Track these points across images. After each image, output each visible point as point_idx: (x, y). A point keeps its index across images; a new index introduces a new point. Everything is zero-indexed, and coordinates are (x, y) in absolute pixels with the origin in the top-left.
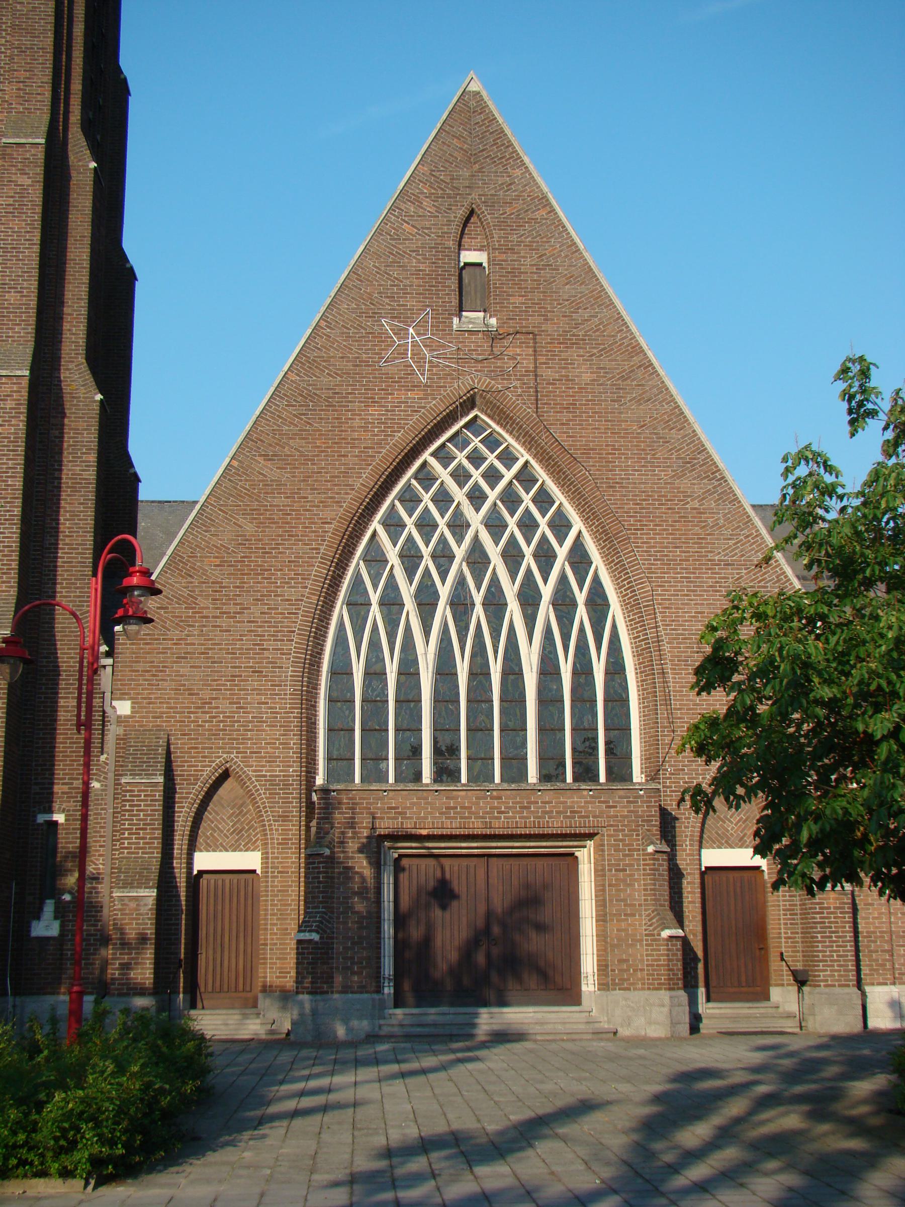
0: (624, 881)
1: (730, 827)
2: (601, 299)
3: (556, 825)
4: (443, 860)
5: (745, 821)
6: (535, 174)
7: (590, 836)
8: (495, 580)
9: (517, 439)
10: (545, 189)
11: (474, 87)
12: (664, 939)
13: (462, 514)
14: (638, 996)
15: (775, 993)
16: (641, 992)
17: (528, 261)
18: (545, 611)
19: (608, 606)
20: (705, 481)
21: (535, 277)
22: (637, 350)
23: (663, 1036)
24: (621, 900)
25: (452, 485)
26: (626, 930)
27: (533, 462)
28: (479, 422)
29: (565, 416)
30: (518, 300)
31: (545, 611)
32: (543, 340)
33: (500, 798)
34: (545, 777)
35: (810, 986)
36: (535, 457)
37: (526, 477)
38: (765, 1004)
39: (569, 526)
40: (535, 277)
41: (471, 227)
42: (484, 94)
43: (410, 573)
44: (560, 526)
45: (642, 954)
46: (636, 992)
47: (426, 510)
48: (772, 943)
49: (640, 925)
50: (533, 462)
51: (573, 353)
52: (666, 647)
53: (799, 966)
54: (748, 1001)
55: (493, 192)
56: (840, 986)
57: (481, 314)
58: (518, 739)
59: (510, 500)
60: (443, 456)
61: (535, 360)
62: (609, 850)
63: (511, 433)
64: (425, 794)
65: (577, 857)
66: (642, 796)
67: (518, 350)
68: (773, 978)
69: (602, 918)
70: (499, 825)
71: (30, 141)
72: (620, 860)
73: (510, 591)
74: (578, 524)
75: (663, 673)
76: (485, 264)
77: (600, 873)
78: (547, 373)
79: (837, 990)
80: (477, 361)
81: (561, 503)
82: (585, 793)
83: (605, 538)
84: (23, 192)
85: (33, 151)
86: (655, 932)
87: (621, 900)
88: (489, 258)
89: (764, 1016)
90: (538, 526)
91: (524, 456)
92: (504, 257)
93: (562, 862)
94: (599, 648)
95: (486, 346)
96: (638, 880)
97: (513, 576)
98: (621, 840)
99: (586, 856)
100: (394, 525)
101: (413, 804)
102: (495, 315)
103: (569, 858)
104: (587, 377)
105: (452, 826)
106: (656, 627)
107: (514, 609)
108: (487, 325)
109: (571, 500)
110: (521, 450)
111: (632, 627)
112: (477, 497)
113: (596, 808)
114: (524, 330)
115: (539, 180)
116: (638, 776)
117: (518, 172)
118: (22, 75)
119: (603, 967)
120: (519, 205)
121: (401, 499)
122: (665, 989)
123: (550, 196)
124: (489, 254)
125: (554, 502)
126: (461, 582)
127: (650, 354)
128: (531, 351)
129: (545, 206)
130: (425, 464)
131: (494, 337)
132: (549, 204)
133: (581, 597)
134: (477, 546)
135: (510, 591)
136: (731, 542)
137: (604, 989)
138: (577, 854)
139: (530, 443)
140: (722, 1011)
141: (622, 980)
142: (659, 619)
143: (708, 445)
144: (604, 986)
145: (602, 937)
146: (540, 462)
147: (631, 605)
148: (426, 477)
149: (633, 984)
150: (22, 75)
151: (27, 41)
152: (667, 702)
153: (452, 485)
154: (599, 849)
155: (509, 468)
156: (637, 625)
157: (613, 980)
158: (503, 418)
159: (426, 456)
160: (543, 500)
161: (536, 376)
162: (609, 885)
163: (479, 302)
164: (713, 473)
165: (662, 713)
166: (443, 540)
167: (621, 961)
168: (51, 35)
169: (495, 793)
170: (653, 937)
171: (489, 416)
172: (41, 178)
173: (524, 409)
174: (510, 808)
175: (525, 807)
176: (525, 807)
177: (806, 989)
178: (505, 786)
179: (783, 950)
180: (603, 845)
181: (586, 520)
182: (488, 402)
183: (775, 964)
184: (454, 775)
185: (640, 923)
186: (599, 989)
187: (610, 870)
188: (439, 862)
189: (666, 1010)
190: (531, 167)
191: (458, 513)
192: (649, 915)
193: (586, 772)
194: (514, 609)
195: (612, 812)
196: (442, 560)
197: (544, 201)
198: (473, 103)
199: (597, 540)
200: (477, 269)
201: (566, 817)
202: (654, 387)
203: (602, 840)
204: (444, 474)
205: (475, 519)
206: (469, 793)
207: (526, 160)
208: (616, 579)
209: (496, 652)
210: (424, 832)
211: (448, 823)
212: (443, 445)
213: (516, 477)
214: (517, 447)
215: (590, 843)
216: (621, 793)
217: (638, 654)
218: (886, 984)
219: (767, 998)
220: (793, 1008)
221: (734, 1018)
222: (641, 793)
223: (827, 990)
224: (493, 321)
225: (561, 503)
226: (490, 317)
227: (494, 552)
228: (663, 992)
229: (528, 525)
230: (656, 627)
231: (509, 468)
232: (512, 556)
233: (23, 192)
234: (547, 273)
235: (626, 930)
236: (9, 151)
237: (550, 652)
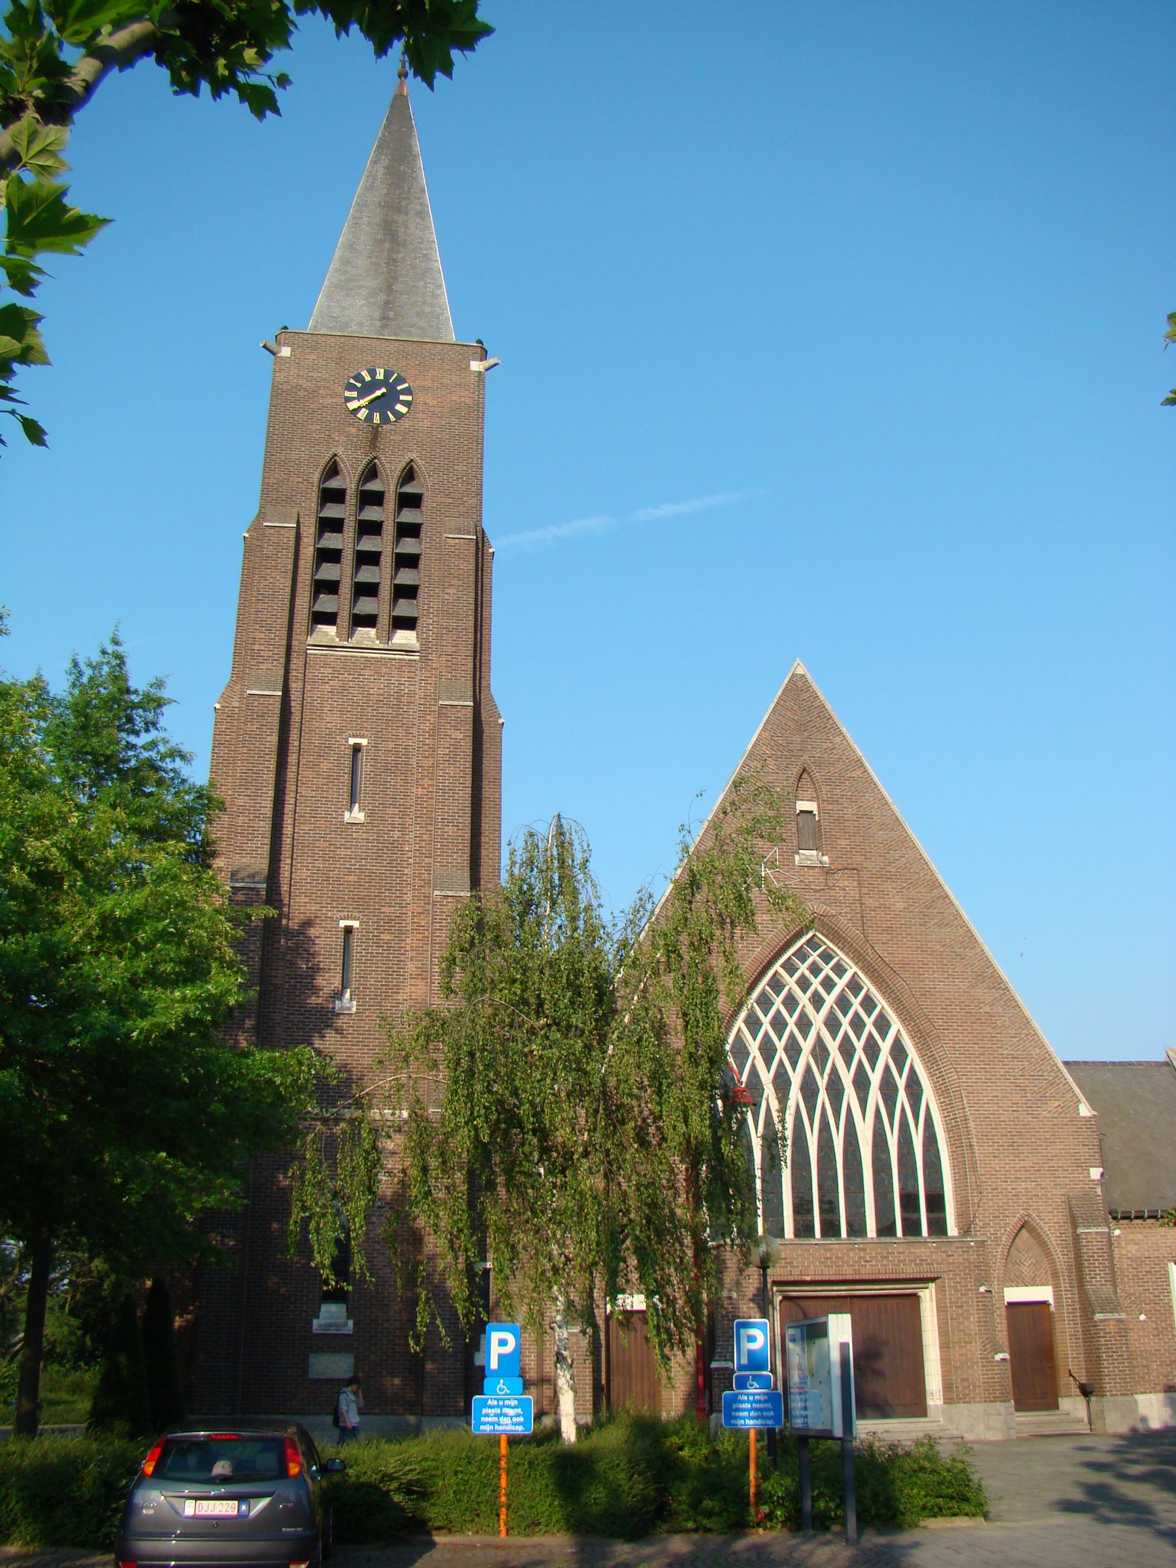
0: (962, 1315)
1: (1024, 1269)
2: (906, 842)
3: (909, 1271)
4: (803, 1303)
5: (1035, 1265)
6: (851, 741)
7: (932, 1280)
8: (834, 1070)
9: (847, 954)
10: (860, 754)
11: (800, 671)
12: (997, 1361)
13: (806, 1015)
14: (979, 1408)
15: (1065, 1403)
16: (980, 1404)
17: (849, 811)
18: (875, 1095)
19: (921, 1091)
20: (993, 990)
21: (856, 824)
22: (936, 884)
23: (1000, 1438)
24: (961, 1331)
25: (797, 991)
26: (965, 1355)
27: (860, 973)
28: (816, 939)
29: (885, 937)
30: (844, 842)
31: (875, 1095)
32: (865, 875)
33: (864, 1249)
34: (798, 1233)
35: (1096, 1396)
36: (861, 969)
37: (854, 985)
38: (1056, 1412)
39: (889, 1026)
40: (856, 824)
41: (803, 781)
42: (809, 677)
43: (768, 1063)
44: (883, 1025)
45: (977, 1373)
46: (976, 1405)
47: (778, 1011)
48: (1060, 1362)
49: (976, 1350)
50: (860, 973)
51: (888, 886)
52: (972, 1125)
53: (1083, 1380)
54: (1040, 1409)
55: (819, 755)
56: (1122, 1395)
57: (814, 852)
58: (858, 1200)
59: (843, 1004)
60: (790, 968)
61: (860, 891)
62: (950, 1290)
63: (841, 950)
64: (807, 1247)
65: (919, 1297)
66: (972, 1247)
67: (846, 883)
68: (1063, 1390)
69: (945, 1346)
70: (866, 1272)
71: (461, 703)
72: (958, 1298)
73: (847, 1078)
74: (896, 1025)
75: (971, 1146)
76: (816, 812)
77: (941, 1309)
78: (870, 902)
79: (1120, 1398)
80: (815, 891)
81: (883, 1007)
82: (930, 1245)
83: (919, 1037)
84: (456, 744)
85: (464, 712)
86: (990, 1356)
87: (961, 1331)
88: (819, 808)
89: (1062, 1421)
90: (865, 1025)
91: (852, 969)
92: (831, 807)
93: (907, 1302)
94: (917, 1125)
95: (822, 879)
96: (973, 1314)
97: (848, 1065)
98: (958, 1283)
99: (928, 1297)
100: (753, 1024)
101: (798, 1255)
102: (827, 854)
103: (913, 1298)
104: (900, 906)
105: (829, 1273)
106: (964, 1108)
107: (850, 1094)
108: (821, 862)
109: (891, 1004)
110: (850, 963)
111: (943, 1107)
112: (817, 1001)
113: (938, 1256)
114: (850, 867)
115: (855, 746)
116: (952, 1230)
117: (837, 740)
118: (450, 649)
119: (947, 1386)
120: (840, 766)
121: (758, 1002)
122: (1001, 1401)
123: (863, 759)
124: (818, 805)
125: (876, 1006)
126: (808, 1071)
127: (946, 888)
128: (856, 884)
129: (860, 767)
130: (776, 972)
131: (828, 872)
132: (862, 766)
133: (901, 1083)
134: (819, 1042)
135: (847, 1078)
136: (1015, 1040)
137: (950, 1403)
138: (920, 1294)
139: (858, 958)
140: (1030, 1419)
141: (965, 1395)
142: (965, 1102)
143: (995, 962)
144: (948, 1400)
145: (945, 1361)
146: (866, 973)
147: (942, 1091)
148: (777, 984)
149: (974, 1398)
150: (450, 649)
151: (452, 623)
152: (974, 1169)
153: (797, 991)
154: (940, 1291)
155: (840, 977)
156: (947, 1107)
157: (958, 1395)
158: (837, 936)
159: (777, 967)
160: (869, 1004)
161: (861, 904)
162: (952, 1319)
163: (811, 842)
164: (998, 983)
165: (971, 1179)
166: (792, 1036)
167: (964, 1380)
168: (471, 618)
169: (861, 1246)
170: (988, 1361)
171: (824, 935)
172: (470, 733)
173: (853, 931)
174: (873, 1257)
175: (885, 1257)
176: (885, 1257)
177: (1093, 1399)
178: (797, 1241)
179: (1071, 1367)
180: (945, 1287)
181: (903, 1021)
182: (824, 925)
183: (1063, 1379)
184: (836, 1233)
185: (976, 1349)
186: (944, 1403)
187: (951, 1307)
188: (798, 1305)
189: (1002, 1418)
190: (848, 736)
191: (803, 1015)
192: (983, 1342)
193: (830, 1228)
194: (850, 1094)
195: (951, 1259)
196: (792, 1052)
197: (859, 764)
198: (800, 684)
199: (912, 1037)
200: (809, 816)
201: (916, 1265)
202: (950, 914)
203: (944, 1282)
204: (791, 982)
205: (818, 1020)
206: (842, 1246)
207: (844, 730)
208: (928, 1069)
209: (838, 1128)
210: (808, 1278)
211: (826, 1271)
212: (789, 958)
213: (848, 986)
214: (847, 960)
215: (932, 1286)
216: (957, 1244)
217: (949, 1130)
218: (1146, 1393)
219: (1056, 1407)
220: (1082, 1413)
221: (1037, 1424)
222: (972, 1244)
223: (1112, 1398)
224: (826, 859)
225: (883, 1007)
226: (823, 855)
227: (833, 1046)
228: (998, 1404)
229: (857, 1024)
230: (964, 1108)
231: (840, 977)
232: (847, 1050)
233: (456, 744)
234: (864, 821)
235: (965, 1355)
236: (444, 711)
237: (879, 1128)
